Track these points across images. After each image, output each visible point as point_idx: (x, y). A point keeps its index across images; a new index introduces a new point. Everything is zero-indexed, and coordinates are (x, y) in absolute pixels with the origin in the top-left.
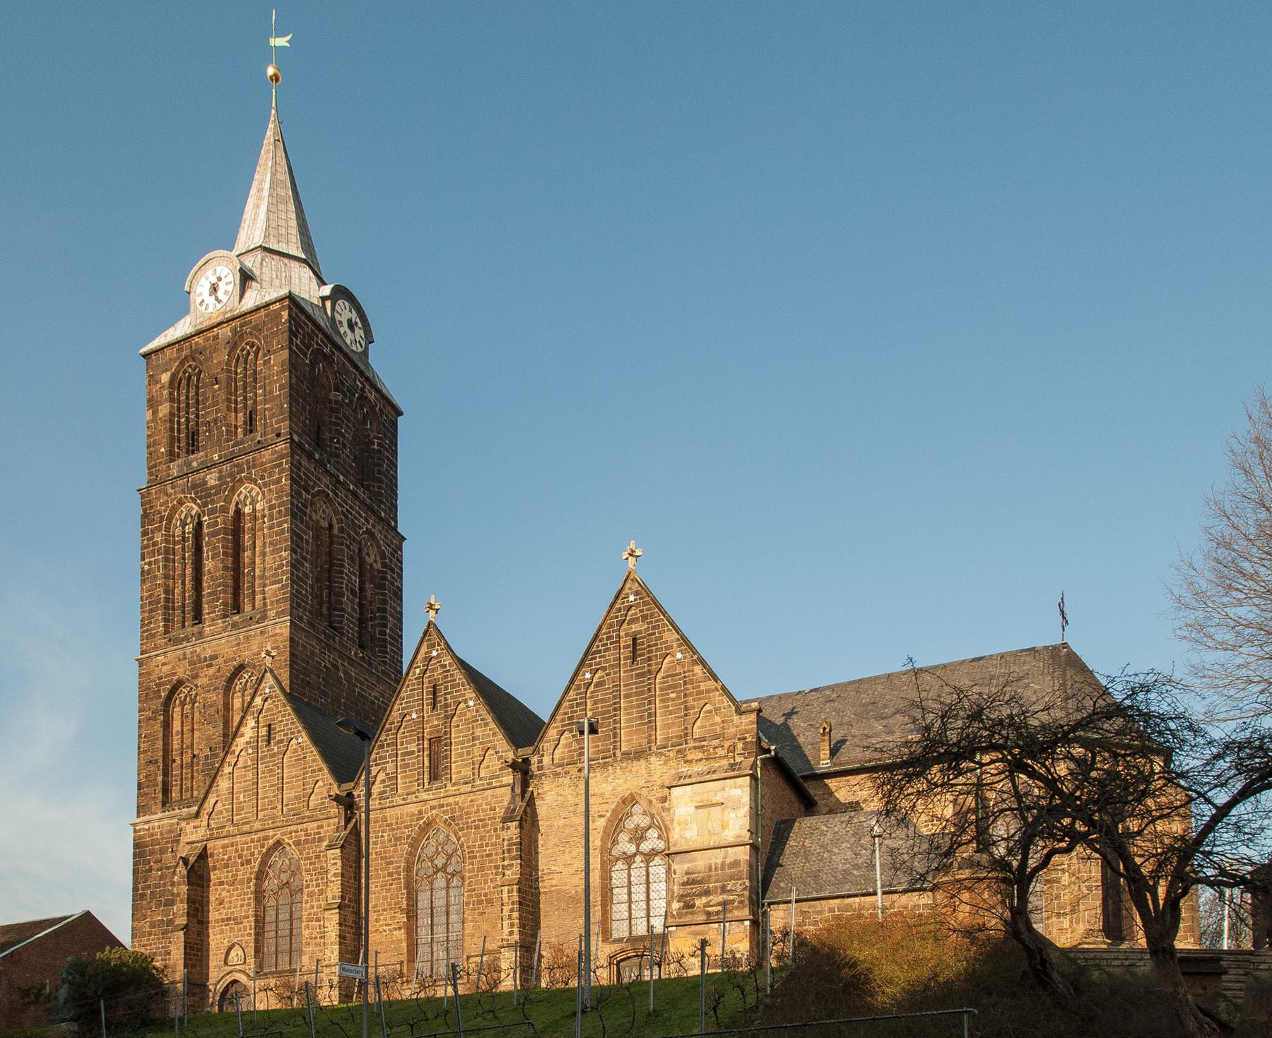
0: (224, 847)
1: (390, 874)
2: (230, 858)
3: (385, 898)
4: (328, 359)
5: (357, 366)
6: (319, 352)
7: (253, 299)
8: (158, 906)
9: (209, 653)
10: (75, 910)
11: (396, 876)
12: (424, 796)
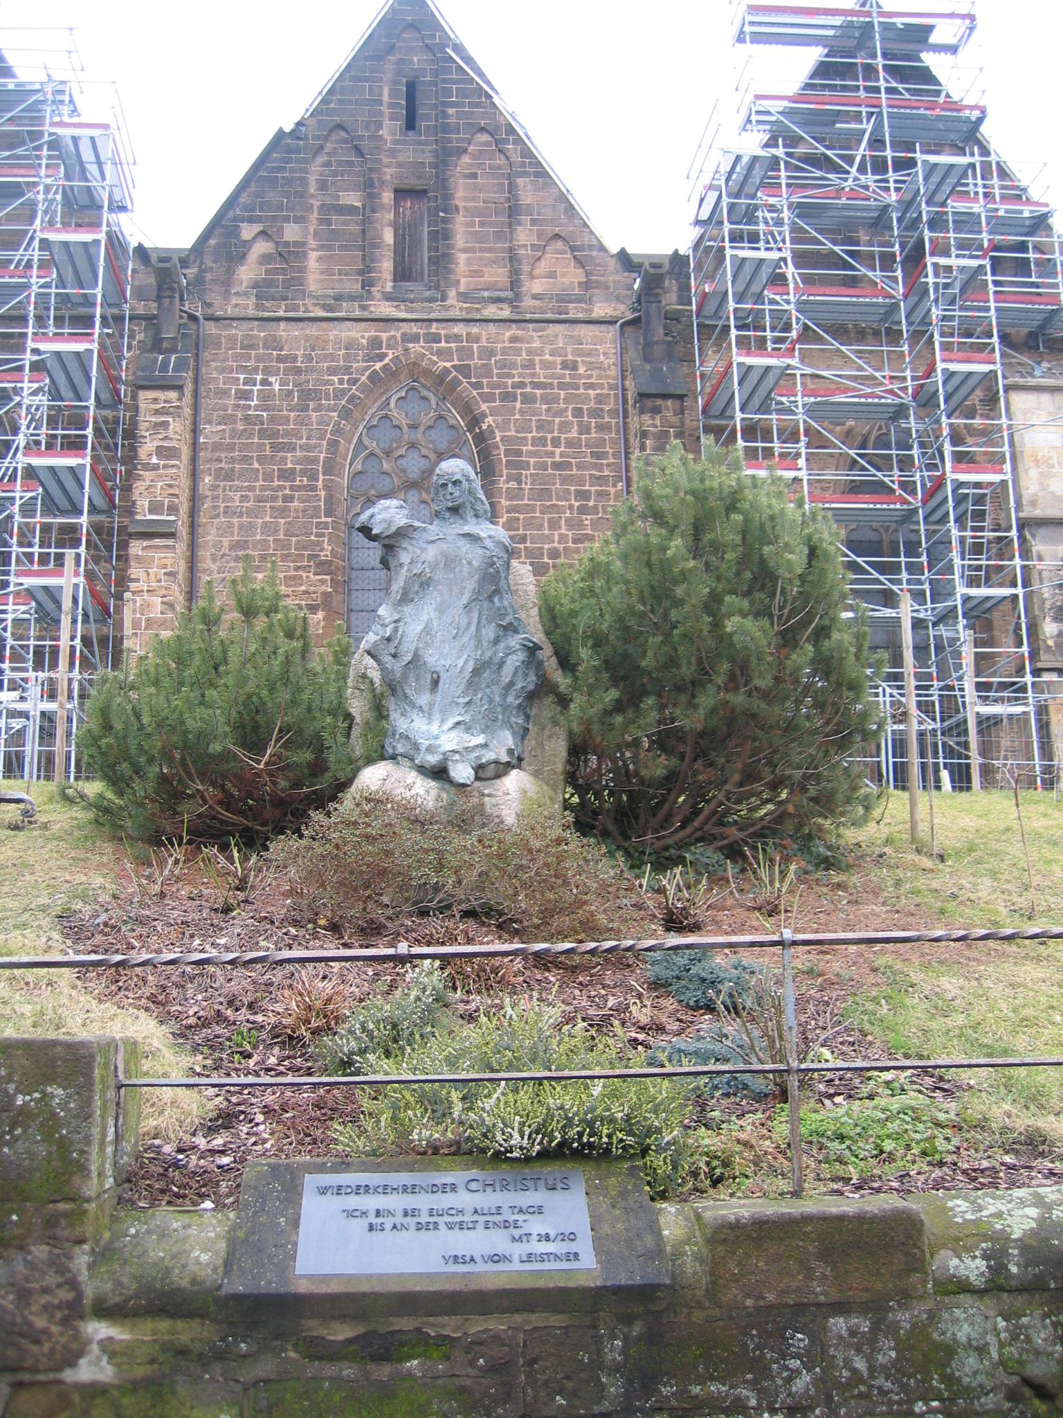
1: (285, 475)
3: (269, 529)
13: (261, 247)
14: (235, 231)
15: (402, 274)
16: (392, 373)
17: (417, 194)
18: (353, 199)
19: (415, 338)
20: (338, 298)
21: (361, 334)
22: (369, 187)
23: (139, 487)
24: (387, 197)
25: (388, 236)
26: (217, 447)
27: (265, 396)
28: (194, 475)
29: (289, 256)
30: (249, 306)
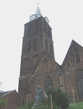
0: (38, 78)
1: (71, 79)
2: (39, 79)
3: (71, 84)
4: (45, 23)
5: (48, 24)
6: (44, 22)
7: (37, 18)
8: (22, 90)
9: (31, 54)
10: (13, 90)
11: (73, 80)
12: (76, 65)
13: (67, 63)
14: (65, 63)
15: (77, 62)
16: (78, 70)
17: (77, 56)
18: (72, 58)
19: (79, 67)
20: (73, 65)
21: (75, 68)
22: (73, 57)
23: (60, 83)
24: (75, 57)
25: (75, 60)
26: (66, 78)
27: (69, 74)
28: (65, 81)
29: (69, 63)
30: (67, 68)
